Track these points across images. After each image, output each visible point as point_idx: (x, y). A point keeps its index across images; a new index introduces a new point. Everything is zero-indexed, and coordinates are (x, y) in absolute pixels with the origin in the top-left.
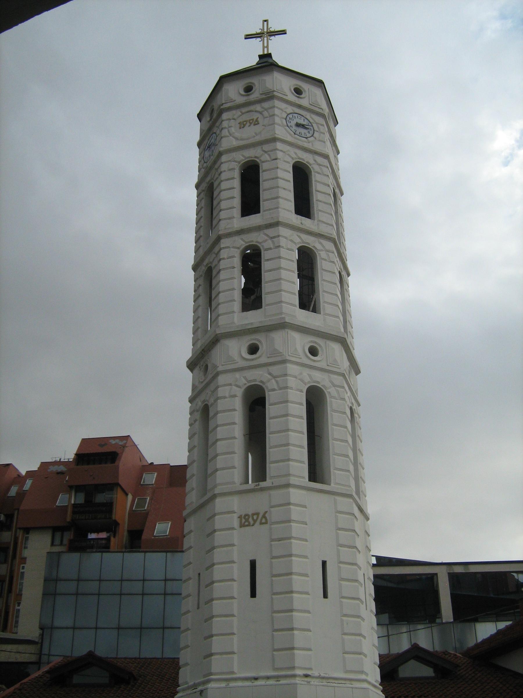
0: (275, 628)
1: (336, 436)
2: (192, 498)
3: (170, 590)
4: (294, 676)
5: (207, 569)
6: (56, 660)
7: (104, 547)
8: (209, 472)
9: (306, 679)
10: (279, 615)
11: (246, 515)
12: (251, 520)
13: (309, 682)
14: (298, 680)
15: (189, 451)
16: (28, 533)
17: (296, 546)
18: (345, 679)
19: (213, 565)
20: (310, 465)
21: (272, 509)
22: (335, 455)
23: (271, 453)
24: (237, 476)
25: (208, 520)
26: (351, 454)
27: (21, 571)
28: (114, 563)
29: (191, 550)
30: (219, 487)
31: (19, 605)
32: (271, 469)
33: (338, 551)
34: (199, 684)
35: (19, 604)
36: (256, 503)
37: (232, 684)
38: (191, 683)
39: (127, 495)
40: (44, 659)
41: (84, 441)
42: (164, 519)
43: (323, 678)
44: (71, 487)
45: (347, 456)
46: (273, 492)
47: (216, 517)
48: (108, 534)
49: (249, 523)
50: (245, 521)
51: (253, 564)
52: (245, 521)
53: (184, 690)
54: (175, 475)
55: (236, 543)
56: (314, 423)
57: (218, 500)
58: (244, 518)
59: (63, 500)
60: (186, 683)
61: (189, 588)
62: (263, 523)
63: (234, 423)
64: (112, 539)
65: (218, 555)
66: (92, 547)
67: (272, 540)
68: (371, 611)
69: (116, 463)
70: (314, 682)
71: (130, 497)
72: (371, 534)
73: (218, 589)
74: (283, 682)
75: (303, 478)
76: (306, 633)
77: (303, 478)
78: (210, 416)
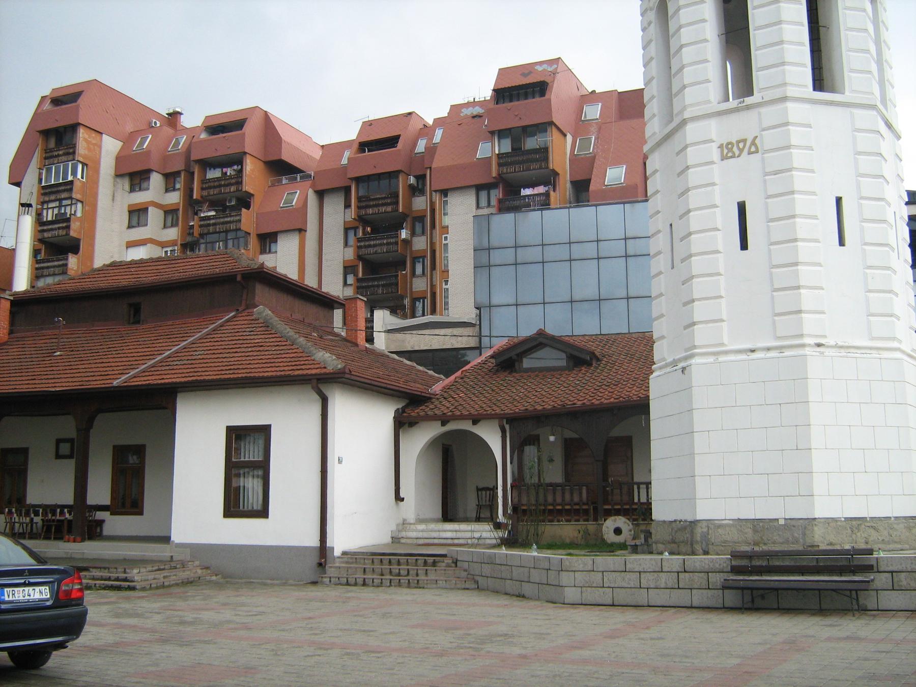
0: (775, 287)
1: (850, 25)
2: (654, 128)
3: (632, 251)
4: (803, 346)
5: (681, 217)
6: (499, 343)
7: (545, 203)
8: (674, 90)
9: (819, 349)
10: (778, 270)
11: (728, 144)
12: (735, 149)
13: (823, 353)
14: (807, 351)
15: (645, 66)
16: (446, 196)
17: (800, 180)
18: (871, 348)
19: (689, 211)
20: (813, 69)
21: (763, 133)
22: (849, 51)
23: (758, 57)
24: (713, 92)
25: (678, 154)
26: (873, 48)
27: (444, 242)
28: (558, 221)
29: (658, 175)
30: (689, 110)
31: (446, 284)
32: (760, 78)
33: (860, 205)
34: (680, 360)
35: (446, 282)
36: (741, 126)
37: (722, 358)
38: (669, 360)
39: (565, 135)
40: (485, 341)
41: (503, 72)
42: (616, 163)
43: (841, 347)
44: (492, 133)
45: (867, 51)
46: (763, 110)
47: (689, 149)
48: (547, 188)
49: (734, 153)
50: (729, 151)
51: (742, 208)
52: (729, 151)
53: (661, 368)
54: (629, 104)
55: (717, 182)
56: (817, 9)
57: (689, 127)
58: (727, 148)
59: (487, 150)
60: (664, 359)
61: (660, 243)
62: (753, 153)
63: (704, 21)
64: (552, 193)
65: (695, 198)
66: (529, 205)
67: (766, 174)
68: (906, 261)
69: (547, 96)
70: (828, 352)
71: (569, 138)
72: (903, 158)
73: (697, 242)
74: (788, 353)
75: (806, 86)
76: (817, 291)
77: (806, 86)
78: (670, 14)
